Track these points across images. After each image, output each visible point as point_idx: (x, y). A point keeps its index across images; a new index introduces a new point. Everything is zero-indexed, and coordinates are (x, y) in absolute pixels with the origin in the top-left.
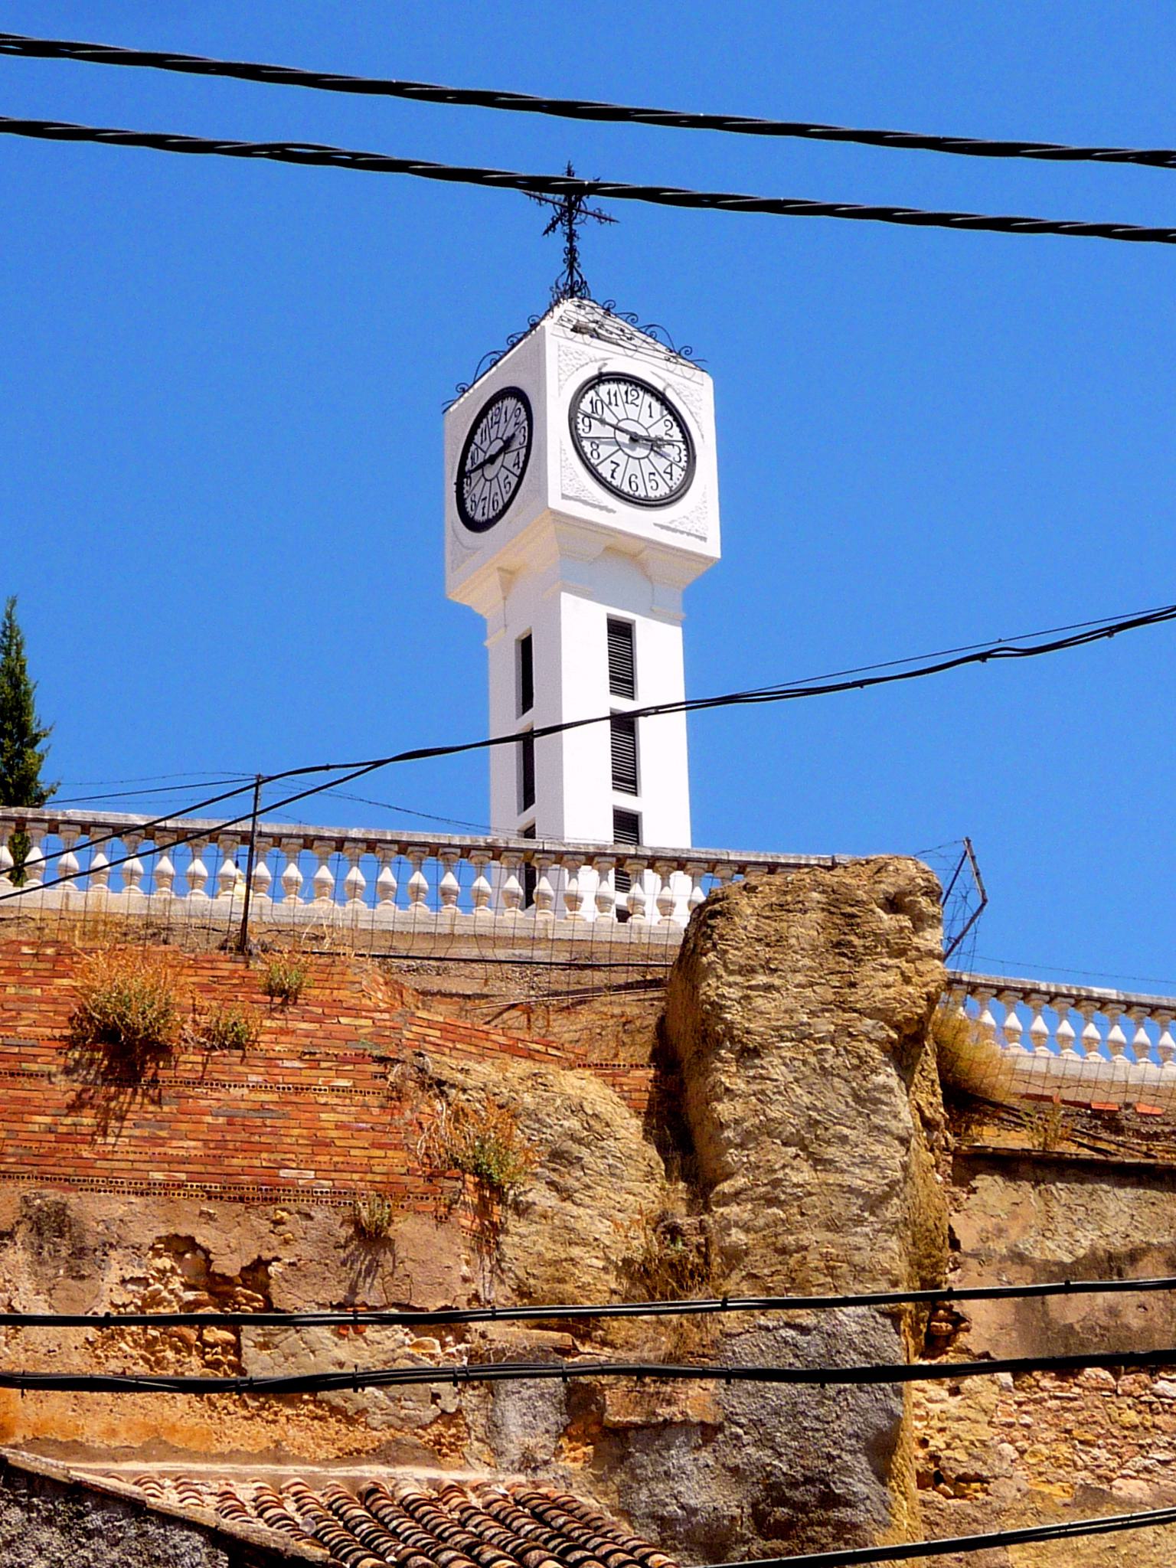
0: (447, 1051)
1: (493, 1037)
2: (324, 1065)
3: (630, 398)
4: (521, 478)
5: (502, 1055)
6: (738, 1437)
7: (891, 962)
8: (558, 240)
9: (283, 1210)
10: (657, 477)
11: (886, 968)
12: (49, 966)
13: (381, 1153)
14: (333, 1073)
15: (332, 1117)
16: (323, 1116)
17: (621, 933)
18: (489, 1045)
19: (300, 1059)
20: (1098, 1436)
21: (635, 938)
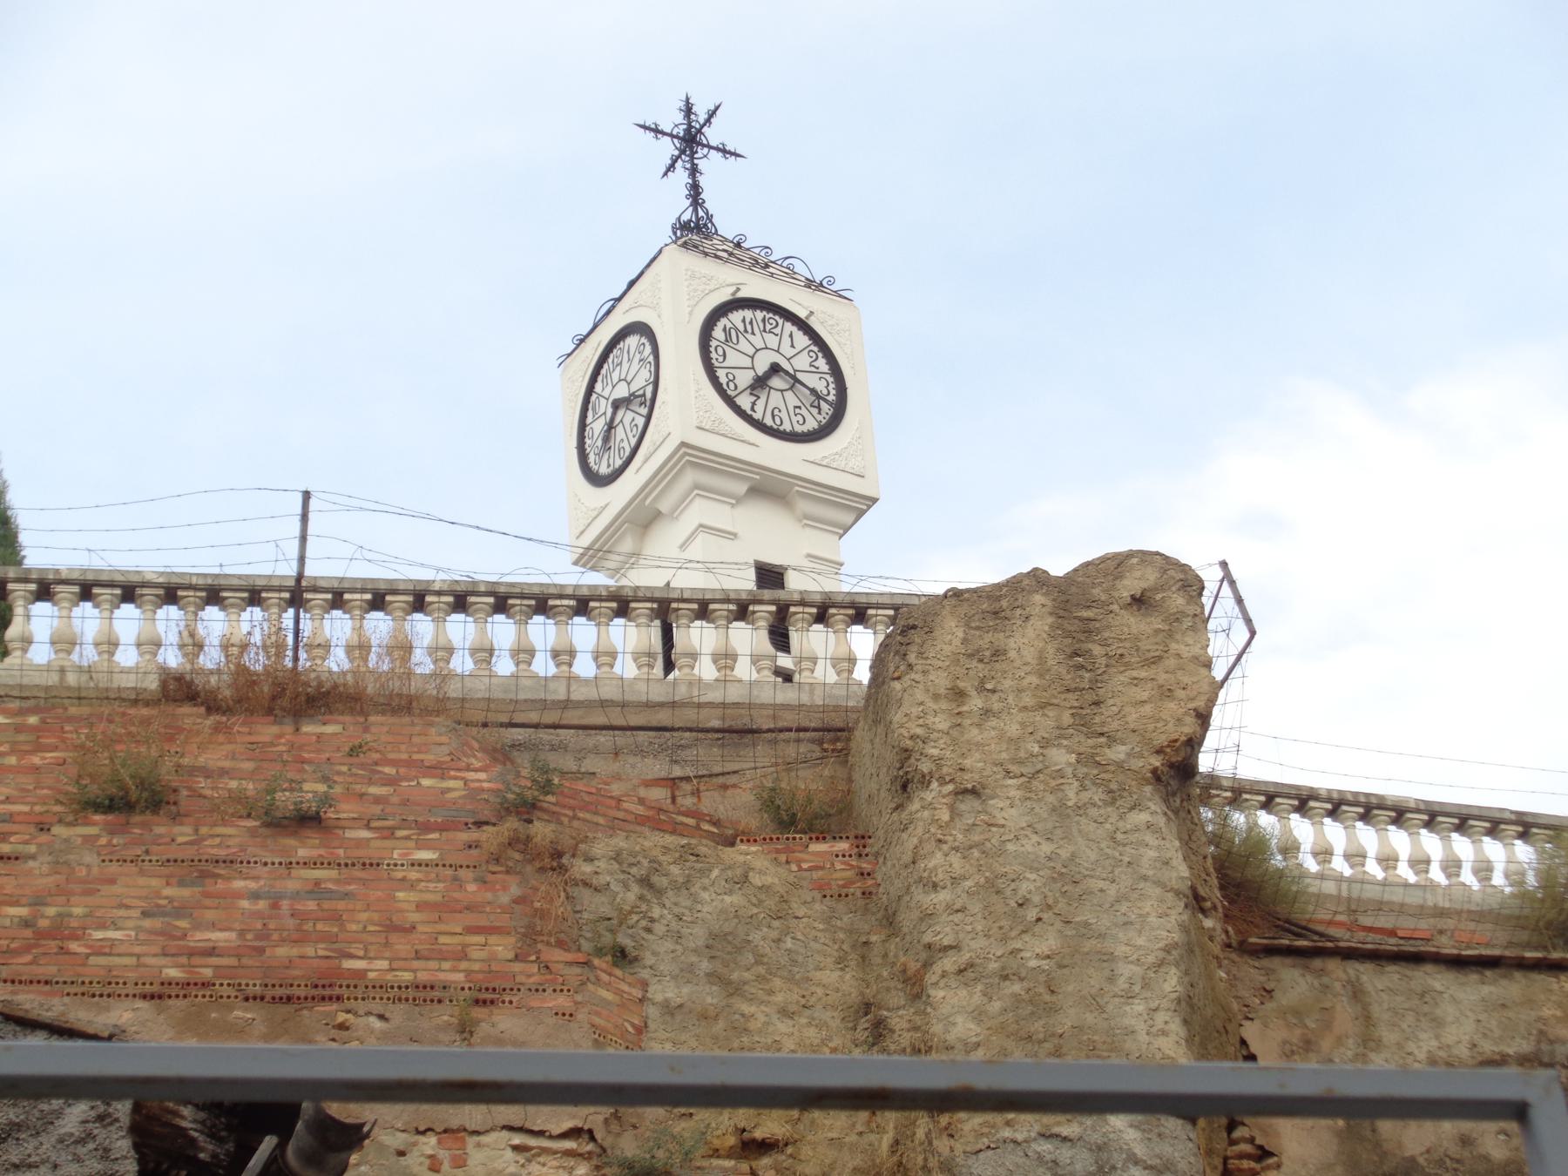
0: (565, 820)
1: (625, 805)
2: (400, 833)
3: (768, 327)
4: (648, 418)
5: (638, 828)
7: (1143, 674)
8: (681, 176)
9: (348, 1012)
10: (804, 411)
11: (1135, 681)
12: (32, 738)
13: (479, 939)
14: (411, 844)
15: (413, 896)
16: (401, 895)
17: (787, 695)
18: (621, 815)
19: (368, 827)
21: (805, 699)
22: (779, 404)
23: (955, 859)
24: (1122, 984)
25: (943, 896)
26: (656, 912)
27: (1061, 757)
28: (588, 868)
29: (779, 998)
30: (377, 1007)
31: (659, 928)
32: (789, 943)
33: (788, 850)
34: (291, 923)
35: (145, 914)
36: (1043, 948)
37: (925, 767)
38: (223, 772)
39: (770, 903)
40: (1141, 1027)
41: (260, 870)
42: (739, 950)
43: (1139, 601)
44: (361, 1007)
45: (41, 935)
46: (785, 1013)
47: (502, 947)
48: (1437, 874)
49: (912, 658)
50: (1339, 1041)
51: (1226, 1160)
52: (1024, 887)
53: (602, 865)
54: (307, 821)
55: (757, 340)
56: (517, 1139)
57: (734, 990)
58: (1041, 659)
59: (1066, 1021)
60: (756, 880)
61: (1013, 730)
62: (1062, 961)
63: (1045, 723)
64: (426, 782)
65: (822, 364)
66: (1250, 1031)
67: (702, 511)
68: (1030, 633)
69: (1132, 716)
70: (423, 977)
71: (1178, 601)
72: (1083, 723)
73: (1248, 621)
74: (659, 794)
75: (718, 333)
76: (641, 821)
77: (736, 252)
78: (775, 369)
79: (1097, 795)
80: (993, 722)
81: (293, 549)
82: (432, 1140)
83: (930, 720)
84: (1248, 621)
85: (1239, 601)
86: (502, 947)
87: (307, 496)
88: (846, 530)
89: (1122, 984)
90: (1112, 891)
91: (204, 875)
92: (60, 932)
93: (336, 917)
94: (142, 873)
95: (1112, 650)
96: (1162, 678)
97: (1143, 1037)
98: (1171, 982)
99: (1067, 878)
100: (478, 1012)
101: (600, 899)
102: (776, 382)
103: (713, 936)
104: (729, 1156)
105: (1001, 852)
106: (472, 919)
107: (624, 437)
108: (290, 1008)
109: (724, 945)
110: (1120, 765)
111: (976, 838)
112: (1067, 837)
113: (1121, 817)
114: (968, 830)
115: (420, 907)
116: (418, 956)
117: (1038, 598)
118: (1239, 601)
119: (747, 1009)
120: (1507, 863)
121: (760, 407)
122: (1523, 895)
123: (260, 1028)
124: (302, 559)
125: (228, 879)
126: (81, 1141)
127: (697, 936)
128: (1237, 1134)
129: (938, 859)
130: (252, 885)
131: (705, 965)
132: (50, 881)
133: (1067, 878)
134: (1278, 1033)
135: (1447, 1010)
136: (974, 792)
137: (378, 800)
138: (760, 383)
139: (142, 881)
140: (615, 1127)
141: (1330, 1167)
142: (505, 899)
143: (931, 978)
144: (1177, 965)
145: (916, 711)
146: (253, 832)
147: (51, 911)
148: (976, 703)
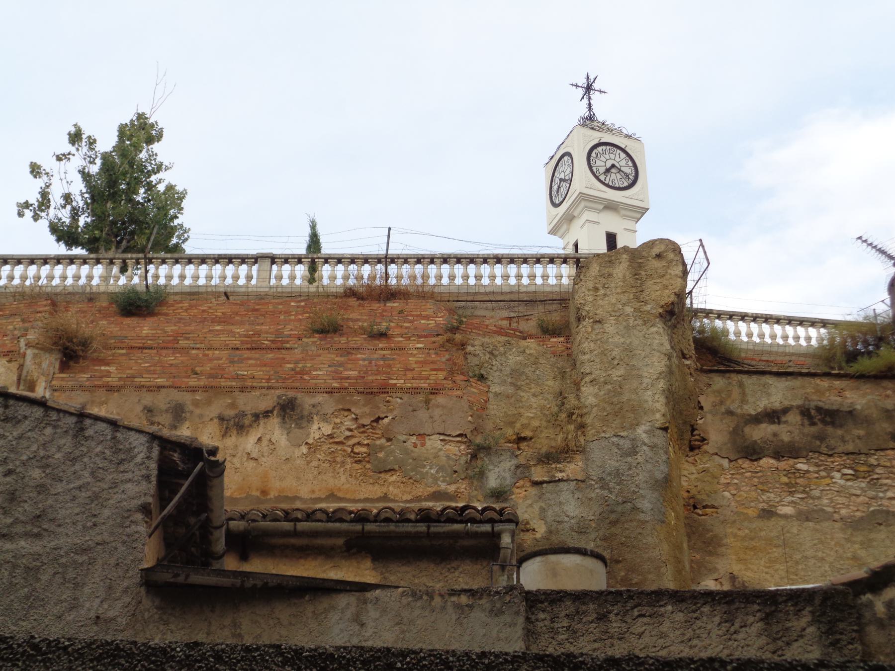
6: (592, 485)
7: (658, 281)
8: (586, 101)
11: (656, 283)
15: (414, 359)
20: (770, 488)
22: (615, 178)
23: (592, 344)
24: (644, 385)
25: (587, 357)
26: (494, 363)
27: (629, 310)
28: (473, 349)
29: (533, 390)
30: (399, 395)
31: (495, 368)
32: (538, 372)
33: (543, 341)
34: (375, 368)
35: (329, 366)
36: (619, 373)
37: (584, 314)
38: (358, 320)
39: (532, 359)
40: (650, 399)
41: (367, 351)
42: (521, 375)
43: (659, 256)
44: (394, 395)
45: (297, 373)
46: (534, 395)
47: (441, 375)
48: (791, 341)
49: (582, 277)
50: (733, 401)
51: (690, 441)
52: (614, 353)
53: (477, 347)
54: (383, 335)
55: (607, 156)
56: (442, 437)
57: (518, 388)
58: (624, 276)
59: (625, 398)
60: (528, 352)
61: (613, 300)
62: (624, 378)
63: (624, 298)
64: (423, 322)
65: (630, 163)
66: (702, 399)
67: (587, 215)
68: (621, 268)
69: (653, 295)
70: (415, 385)
71: (671, 255)
72: (637, 298)
73: (708, 260)
74: (505, 323)
75: (593, 155)
76: (495, 332)
77: (603, 127)
78: (613, 166)
79: (640, 322)
80: (607, 298)
81: (385, 248)
82: (415, 437)
83: (586, 298)
84: (708, 260)
85: (705, 253)
86: (441, 375)
87: (390, 229)
88: (639, 219)
89: (644, 385)
90: (643, 354)
91: (349, 353)
92: (303, 372)
93: (389, 366)
94: (329, 353)
95: (649, 272)
96: (665, 282)
97: (650, 403)
98: (661, 384)
99: (629, 350)
100: (431, 397)
101: (476, 359)
102: (613, 170)
103: (513, 370)
104: (513, 443)
105: (607, 342)
106: (432, 366)
107: (563, 191)
108: (372, 396)
109: (516, 373)
110: (648, 312)
111: (599, 337)
112: (629, 336)
113: (648, 329)
114: (597, 334)
115: (416, 362)
116: (413, 379)
117: (625, 256)
118: (705, 253)
119: (522, 394)
120: (812, 338)
121: (607, 179)
122: (822, 347)
123: (362, 402)
124: (387, 250)
125: (356, 354)
126: (141, 464)
127: (508, 370)
128: (695, 433)
129: (586, 344)
130: (363, 356)
131: (509, 380)
132: (300, 356)
133: (629, 350)
134: (712, 399)
135: (773, 390)
136: (599, 322)
137: (407, 328)
138: (608, 171)
139: (329, 356)
140: (475, 433)
141: (726, 444)
142: (444, 359)
143: (582, 384)
144: (664, 378)
145: (582, 295)
146: (365, 339)
147: (300, 365)
148: (602, 292)
